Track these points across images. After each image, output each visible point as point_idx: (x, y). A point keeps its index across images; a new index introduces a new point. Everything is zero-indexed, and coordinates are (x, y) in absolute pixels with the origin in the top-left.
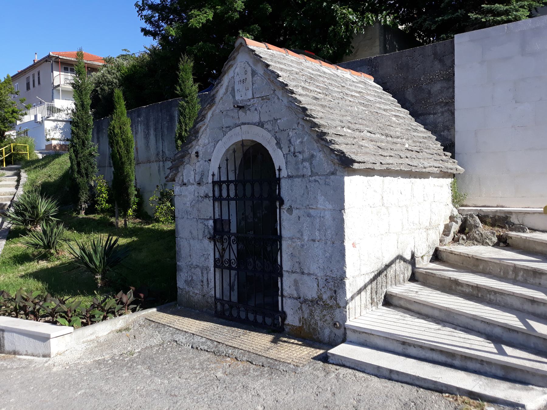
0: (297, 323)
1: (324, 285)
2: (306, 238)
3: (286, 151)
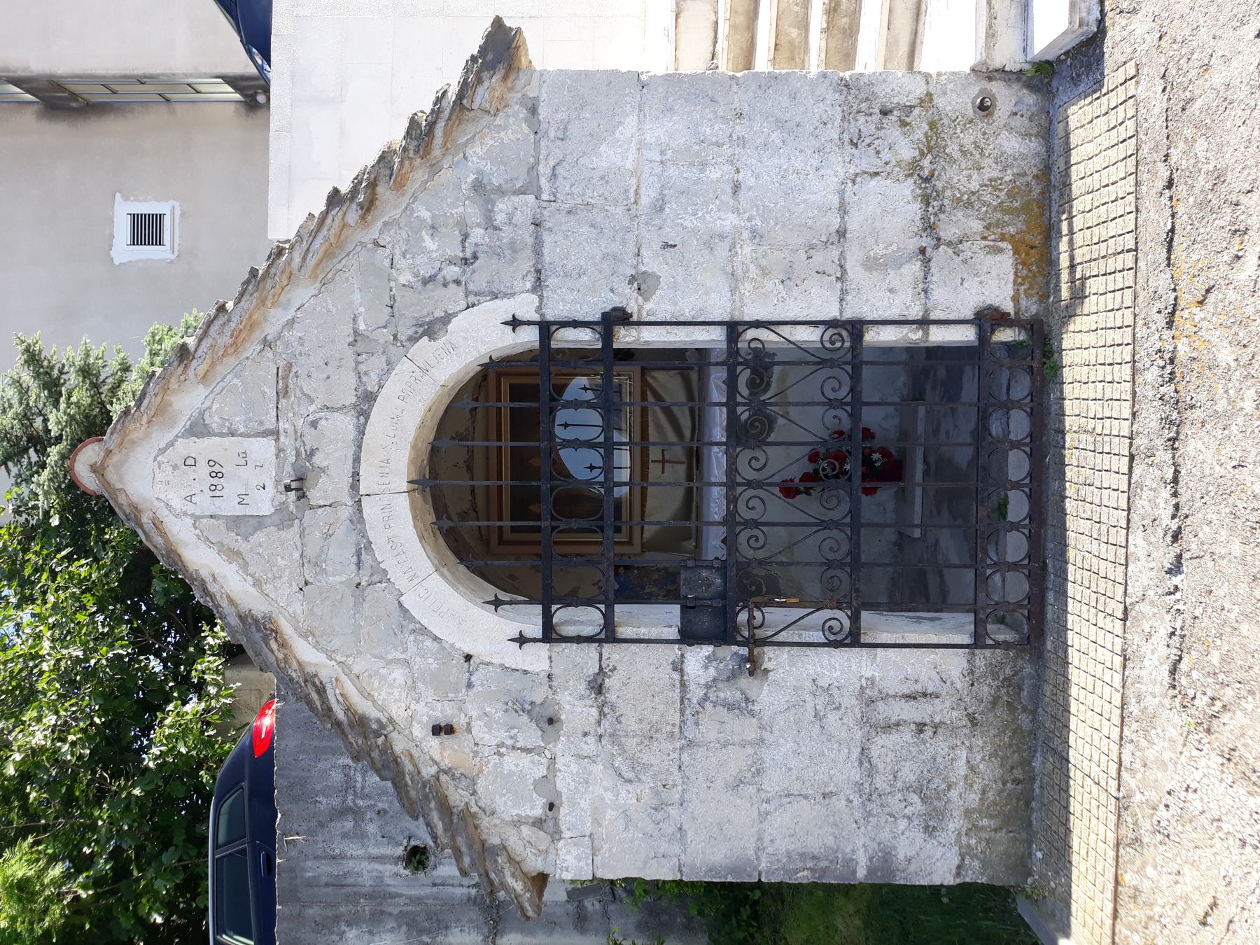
0: (1004, 264)
1: (871, 151)
2: (730, 221)
3: (453, 298)
